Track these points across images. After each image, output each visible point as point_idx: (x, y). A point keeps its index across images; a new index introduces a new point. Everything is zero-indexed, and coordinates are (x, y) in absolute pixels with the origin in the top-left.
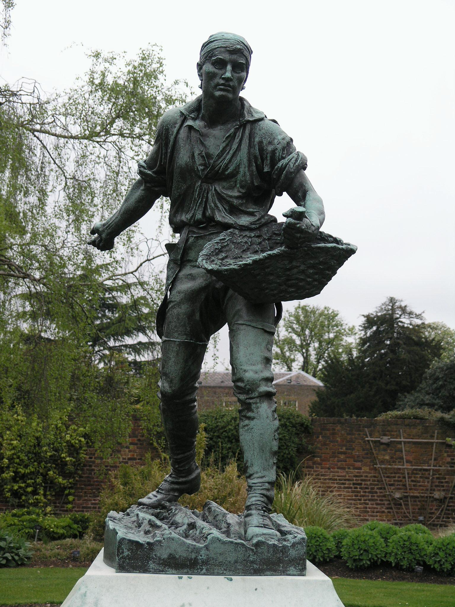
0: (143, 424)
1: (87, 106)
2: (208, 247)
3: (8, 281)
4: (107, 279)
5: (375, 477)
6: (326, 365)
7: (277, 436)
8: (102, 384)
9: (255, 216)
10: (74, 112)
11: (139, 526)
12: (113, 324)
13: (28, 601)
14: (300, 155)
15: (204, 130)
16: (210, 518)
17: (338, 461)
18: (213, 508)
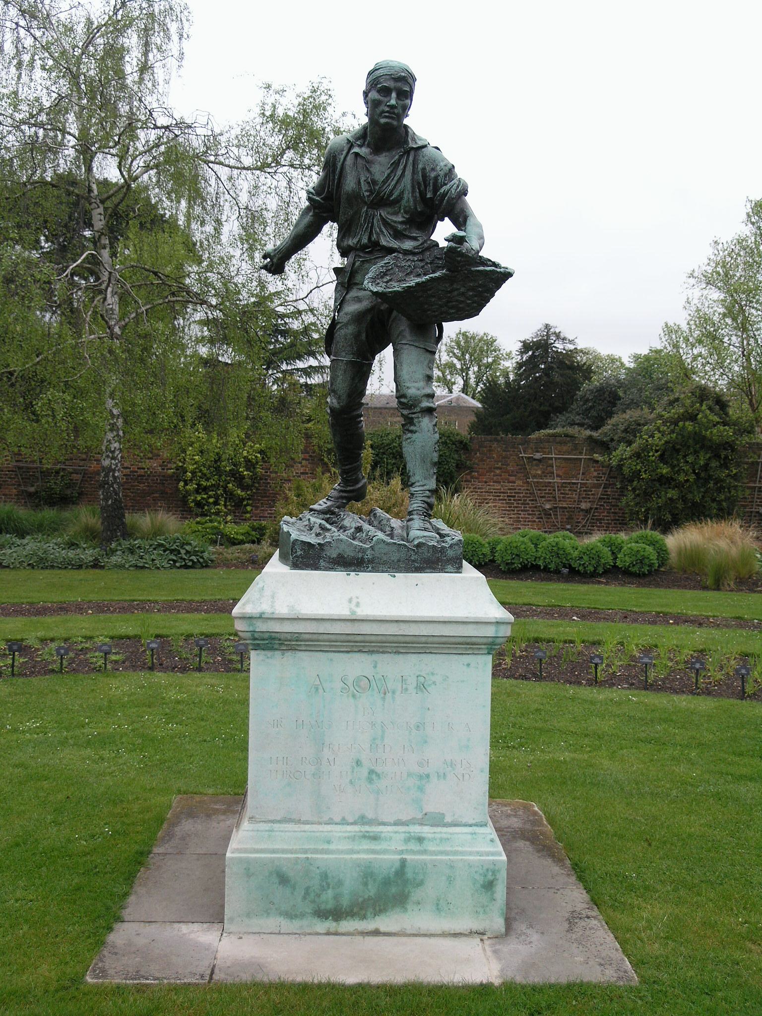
0: (315, 441)
1: (258, 138)
2: (373, 271)
3: (186, 307)
4: (279, 306)
5: (527, 490)
6: (484, 388)
7: (437, 448)
8: (276, 404)
9: (418, 240)
10: (246, 144)
11: (311, 529)
12: (285, 349)
13: (212, 597)
14: (462, 182)
15: (370, 157)
16: (376, 523)
17: (494, 476)
18: (378, 514)
